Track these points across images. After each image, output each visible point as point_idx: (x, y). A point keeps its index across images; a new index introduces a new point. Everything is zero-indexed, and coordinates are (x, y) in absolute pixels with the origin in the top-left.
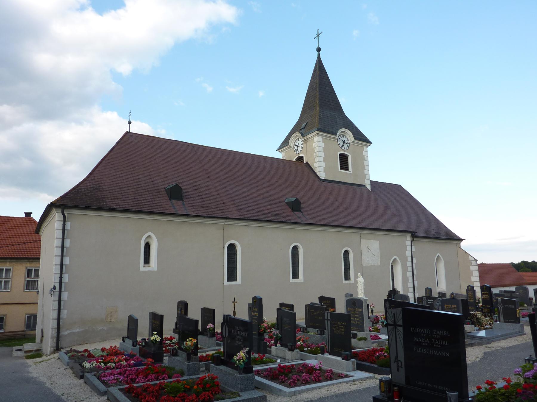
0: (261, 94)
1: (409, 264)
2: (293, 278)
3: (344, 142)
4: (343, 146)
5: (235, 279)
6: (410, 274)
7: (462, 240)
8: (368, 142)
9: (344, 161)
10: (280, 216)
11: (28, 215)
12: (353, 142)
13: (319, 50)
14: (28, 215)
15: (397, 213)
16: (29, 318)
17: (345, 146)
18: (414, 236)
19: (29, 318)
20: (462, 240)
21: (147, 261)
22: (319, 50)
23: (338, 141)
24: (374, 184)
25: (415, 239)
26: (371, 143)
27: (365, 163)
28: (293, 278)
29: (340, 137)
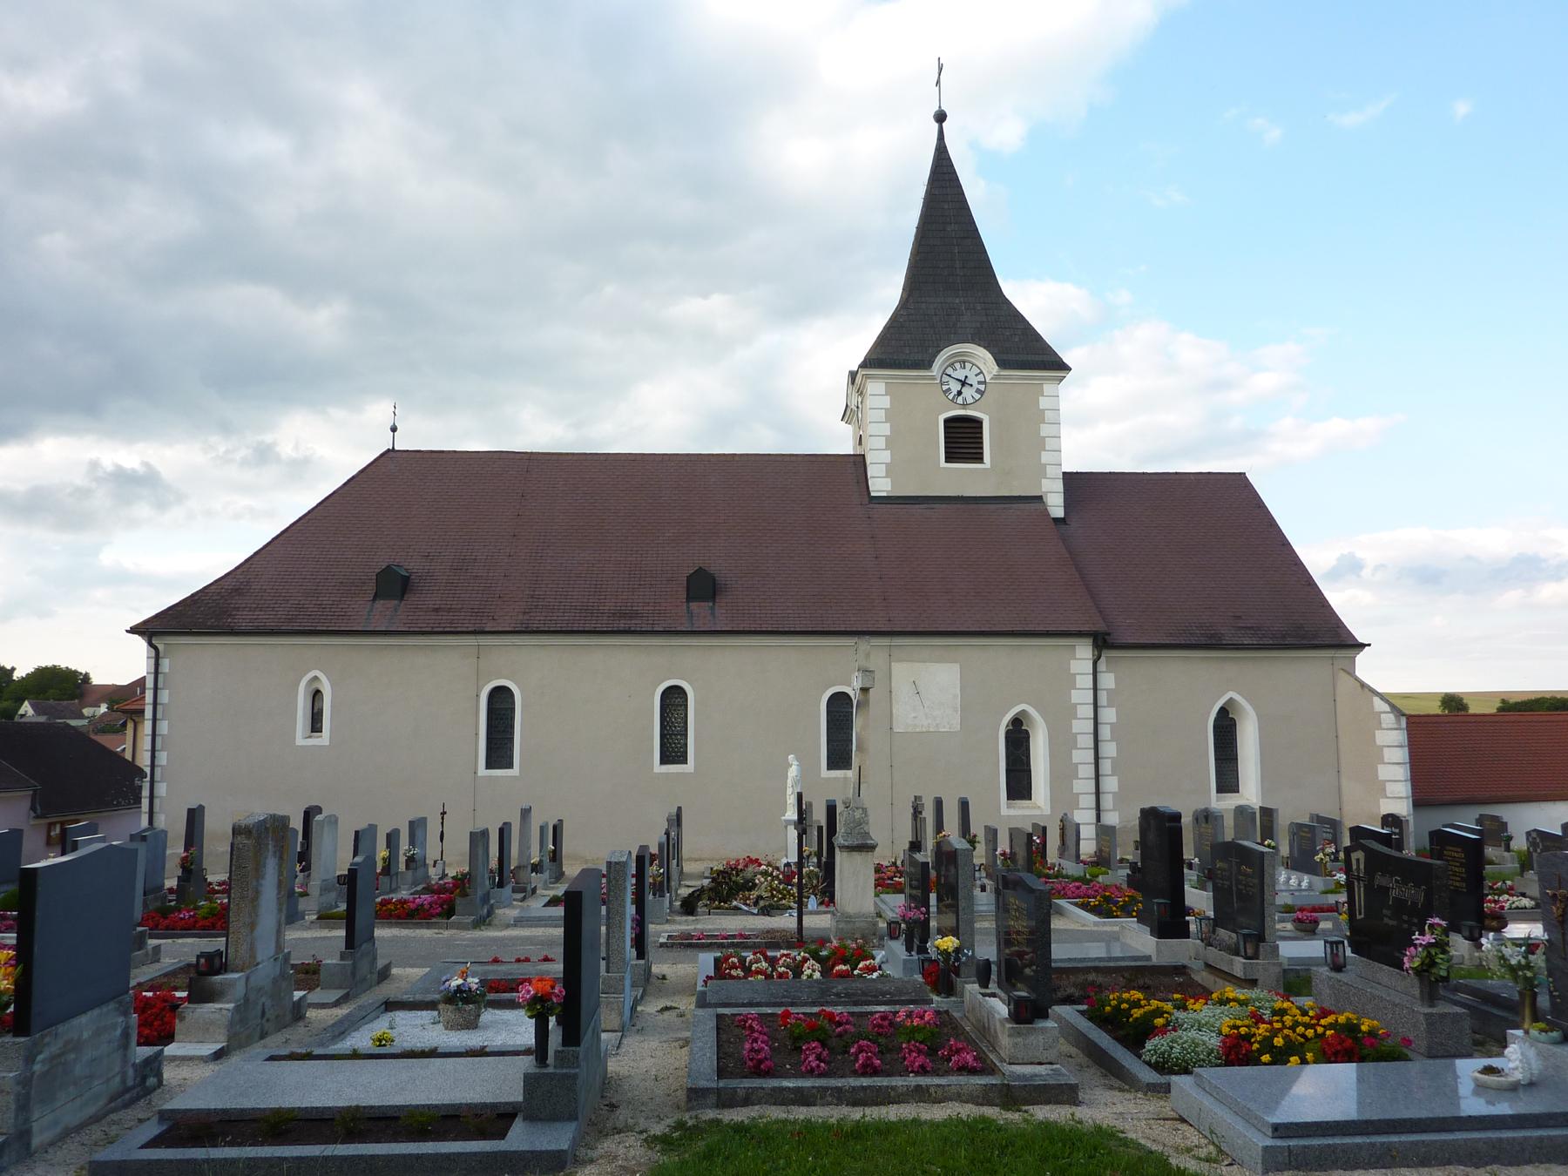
0: (1462, 108)
1: (1082, 726)
2: (665, 760)
3: (964, 383)
4: (960, 393)
5: (683, 759)
6: (1083, 756)
7: (1363, 646)
8: (1055, 365)
9: (963, 439)
10: (634, 615)
11: (13, 669)
12: (996, 377)
13: (941, 117)
14: (13, 669)
15: (1198, 568)
16: (191, 812)
17: (967, 392)
18: (1103, 643)
19: (191, 812)
20: (1363, 646)
21: (316, 725)
22: (941, 117)
23: (942, 384)
24: (1075, 483)
25: (1106, 654)
26: (1066, 368)
27: (1045, 430)
28: (665, 760)
29: (950, 371)
